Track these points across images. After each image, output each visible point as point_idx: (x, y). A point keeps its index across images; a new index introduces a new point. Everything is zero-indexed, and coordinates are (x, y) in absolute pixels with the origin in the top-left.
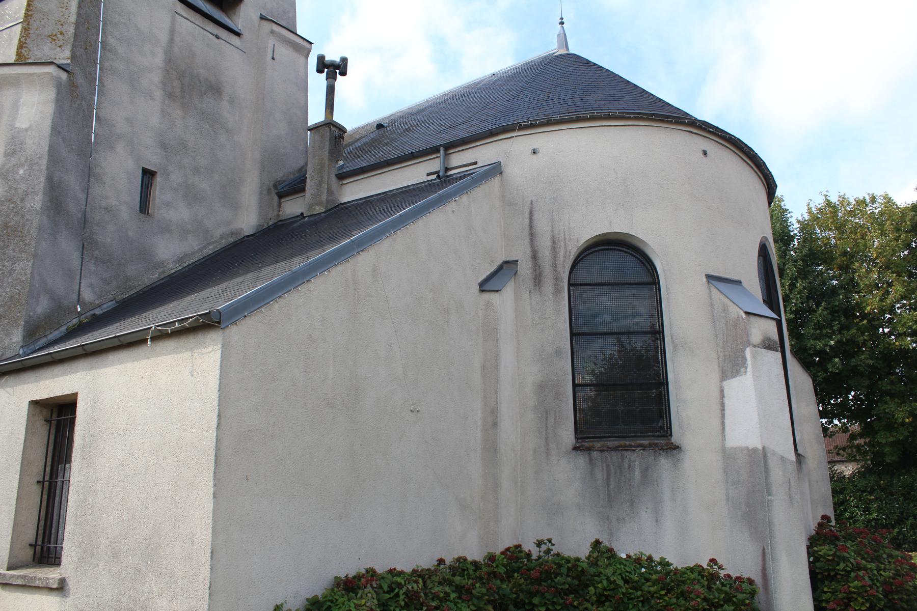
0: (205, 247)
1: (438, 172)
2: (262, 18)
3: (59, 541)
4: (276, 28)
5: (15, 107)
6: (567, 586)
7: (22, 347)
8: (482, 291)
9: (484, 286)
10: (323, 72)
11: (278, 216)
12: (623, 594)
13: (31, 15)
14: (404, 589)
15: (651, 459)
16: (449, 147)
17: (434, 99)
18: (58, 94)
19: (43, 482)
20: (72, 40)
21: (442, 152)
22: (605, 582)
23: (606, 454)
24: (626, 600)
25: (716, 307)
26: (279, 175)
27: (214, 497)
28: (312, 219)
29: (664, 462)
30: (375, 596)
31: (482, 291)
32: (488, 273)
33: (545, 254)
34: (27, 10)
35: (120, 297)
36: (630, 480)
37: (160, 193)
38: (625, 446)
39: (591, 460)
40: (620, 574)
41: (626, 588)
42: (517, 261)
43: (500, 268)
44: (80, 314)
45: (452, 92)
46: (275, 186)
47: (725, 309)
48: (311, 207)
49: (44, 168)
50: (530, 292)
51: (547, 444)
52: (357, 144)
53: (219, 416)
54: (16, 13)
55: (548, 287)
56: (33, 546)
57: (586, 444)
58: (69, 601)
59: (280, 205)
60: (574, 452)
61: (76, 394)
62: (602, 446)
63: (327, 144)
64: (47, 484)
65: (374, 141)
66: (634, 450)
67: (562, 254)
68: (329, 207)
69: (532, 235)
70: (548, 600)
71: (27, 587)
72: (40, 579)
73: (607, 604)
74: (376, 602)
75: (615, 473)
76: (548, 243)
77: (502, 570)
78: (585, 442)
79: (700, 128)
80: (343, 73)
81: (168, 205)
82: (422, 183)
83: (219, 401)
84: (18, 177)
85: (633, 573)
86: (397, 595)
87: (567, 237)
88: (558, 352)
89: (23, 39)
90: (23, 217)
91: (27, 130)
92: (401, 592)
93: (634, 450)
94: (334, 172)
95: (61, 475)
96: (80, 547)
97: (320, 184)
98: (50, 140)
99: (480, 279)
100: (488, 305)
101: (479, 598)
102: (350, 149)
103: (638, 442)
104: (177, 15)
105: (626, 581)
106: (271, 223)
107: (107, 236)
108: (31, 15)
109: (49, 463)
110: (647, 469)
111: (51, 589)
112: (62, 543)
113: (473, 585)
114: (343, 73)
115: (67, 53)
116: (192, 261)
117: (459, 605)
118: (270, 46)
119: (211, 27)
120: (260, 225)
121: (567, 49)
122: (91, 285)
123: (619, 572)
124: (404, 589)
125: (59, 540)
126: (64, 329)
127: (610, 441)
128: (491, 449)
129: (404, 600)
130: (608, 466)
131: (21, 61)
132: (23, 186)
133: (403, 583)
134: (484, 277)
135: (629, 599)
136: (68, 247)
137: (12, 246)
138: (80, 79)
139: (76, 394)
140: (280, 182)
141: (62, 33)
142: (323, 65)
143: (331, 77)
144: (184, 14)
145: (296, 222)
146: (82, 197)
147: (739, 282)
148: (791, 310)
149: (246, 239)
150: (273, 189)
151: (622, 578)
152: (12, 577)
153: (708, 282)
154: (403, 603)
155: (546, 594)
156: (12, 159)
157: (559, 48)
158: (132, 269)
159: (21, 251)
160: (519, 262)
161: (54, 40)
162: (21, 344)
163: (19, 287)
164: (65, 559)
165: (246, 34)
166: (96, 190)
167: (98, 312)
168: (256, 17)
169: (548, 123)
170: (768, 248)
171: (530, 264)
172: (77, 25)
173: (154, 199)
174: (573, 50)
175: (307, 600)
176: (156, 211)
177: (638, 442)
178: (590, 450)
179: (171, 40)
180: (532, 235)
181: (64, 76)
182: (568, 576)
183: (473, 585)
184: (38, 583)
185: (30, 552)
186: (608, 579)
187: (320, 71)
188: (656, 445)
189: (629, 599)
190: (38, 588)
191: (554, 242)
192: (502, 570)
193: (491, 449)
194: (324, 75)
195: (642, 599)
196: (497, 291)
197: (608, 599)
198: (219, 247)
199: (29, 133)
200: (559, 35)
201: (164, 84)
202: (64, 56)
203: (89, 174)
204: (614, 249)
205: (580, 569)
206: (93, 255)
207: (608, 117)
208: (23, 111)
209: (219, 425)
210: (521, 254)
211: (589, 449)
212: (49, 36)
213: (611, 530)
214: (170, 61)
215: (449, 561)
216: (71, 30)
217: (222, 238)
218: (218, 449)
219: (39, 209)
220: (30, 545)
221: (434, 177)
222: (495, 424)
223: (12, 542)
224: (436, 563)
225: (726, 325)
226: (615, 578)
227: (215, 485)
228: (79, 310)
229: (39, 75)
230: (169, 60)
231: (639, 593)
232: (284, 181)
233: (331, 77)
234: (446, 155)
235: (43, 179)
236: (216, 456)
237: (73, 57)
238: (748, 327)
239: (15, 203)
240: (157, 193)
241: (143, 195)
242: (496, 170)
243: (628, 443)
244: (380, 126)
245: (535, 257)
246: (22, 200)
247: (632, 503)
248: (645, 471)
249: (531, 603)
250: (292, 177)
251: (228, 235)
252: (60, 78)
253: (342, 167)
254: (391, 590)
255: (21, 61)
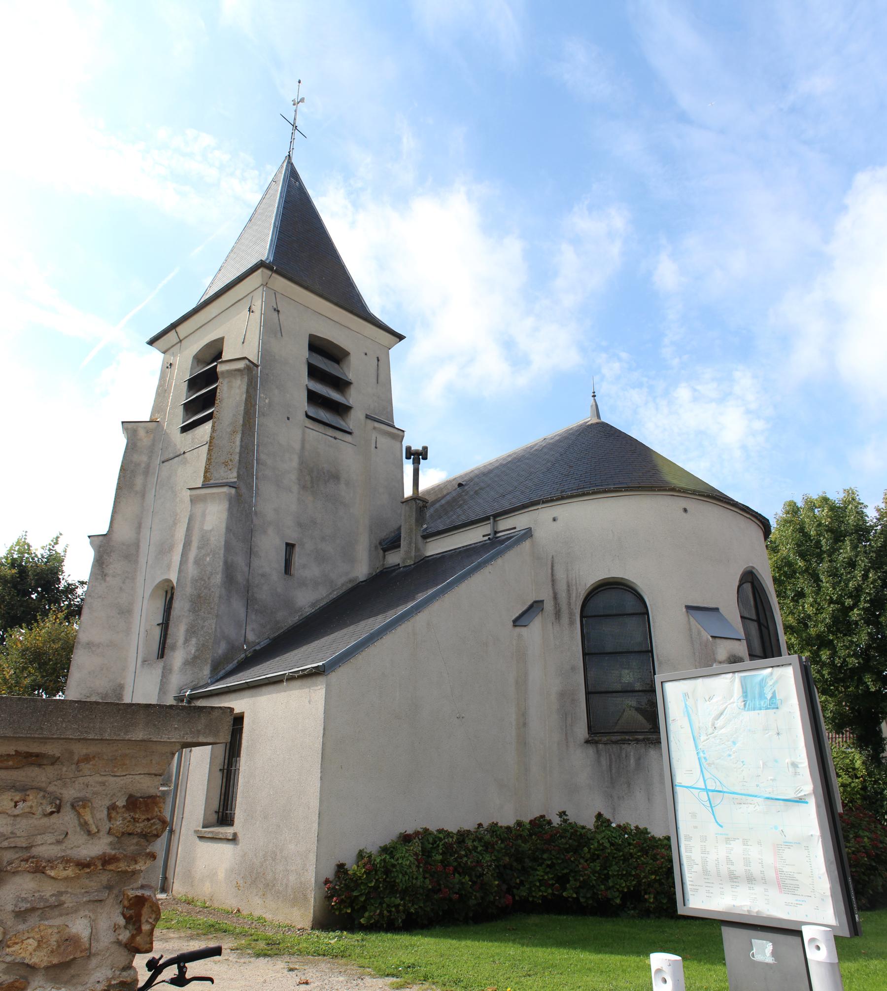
0: (330, 594)
1: (489, 535)
2: (368, 417)
3: (233, 810)
4: (377, 425)
5: (204, 515)
6: (568, 846)
7: (210, 678)
8: (515, 626)
9: (516, 622)
10: (410, 458)
11: (383, 565)
12: (609, 854)
13: (212, 449)
14: (443, 842)
15: (643, 750)
16: (496, 516)
17: (501, 459)
18: (230, 504)
19: (224, 769)
20: (238, 464)
21: (492, 520)
22: (596, 844)
23: (609, 746)
24: (611, 858)
25: (693, 631)
26: (383, 535)
27: (321, 779)
28: (405, 569)
29: (652, 753)
30: (420, 845)
31: (515, 626)
32: (520, 612)
33: (563, 595)
34: (205, 477)
35: (272, 636)
36: (626, 767)
37: (298, 559)
38: (624, 740)
39: (598, 751)
40: (607, 838)
41: (612, 849)
42: (543, 601)
43: (531, 606)
44: (246, 650)
45: (515, 453)
46: (380, 543)
47: (699, 633)
48: (404, 560)
49: (222, 555)
50: (553, 623)
51: (567, 739)
52: (443, 502)
53: (324, 729)
54: (201, 438)
55: (565, 619)
56: (217, 812)
57: (596, 738)
58: (239, 847)
59: (384, 557)
60: (585, 745)
61: (243, 713)
62: (608, 740)
63: (414, 513)
64: (225, 771)
65: (454, 500)
66: (629, 744)
67: (574, 595)
68: (417, 561)
69: (553, 581)
70: (554, 856)
71: (214, 839)
72: (222, 833)
73: (597, 861)
74: (420, 849)
75: (616, 761)
76: (565, 587)
77: (526, 833)
78: (596, 736)
79: (679, 491)
80: (425, 458)
81: (304, 566)
82: (480, 542)
83: (324, 720)
84: (206, 563)
85: (618, 838)
86: (438, 846)
87: (578, 582)
88: (573, 669)
89: (207, 466)
90: (210, 589)
91: (211, 531)
92: (441, 844)
93: (629, 744)
94: (420, 534)
95: (234, 764)
96: (245, 812)
97: (410, 543)
98: (225, 537)
99: (514, 618)
100: (520, 636)
101: (498, 851)
102: (437, 505)
103: (636, 737)
104: (306, 429)
105: (612, 844)
106: (378, 571)
107: (263, 594)
108: (212, 449)
109: (227, 757)
110: (639, 759)
111: (228, 840)
112: (234, 811)
113: (497, 842)
114: (425, 458)
115: (235, 474)
116: (322, 605)
117: (484, 856)
118: (374, 438)
119: (331, 432)
120: (370, 574)
121: (598, 416)
122: (253, 630)
123: (607, 837)
124: (443, 842)
125: (232, 808)
126: (236, 661)
127: (614, 736)
128: (523, 742)
129: (442, 849)
130: (610, 755)
131: (204, 486)
132: (209, 569)
133: (443, 837)
134: (517, 615)
135: (613, 858)
136: (238, 606)
137: (203, 610)
138: (243, 490)
139: (243, 713)
140: (384, 540)
141: (231, 460)
142: (410, 453)
143: (416, 462)
144: (311, 427)
145: (394, 570)
146: (246, 569)
147: (716, 610)
148: (865, 599)
149: (361, 584)
150: (379, 546)
151: (609, 841)
152: (205, 832)
153: (687, 612)
154: (441, 851)
155: (553, 851)
156: (203, 551)
157: (591, 417)
158: (280, 615)
159: (209, 613)
160: (545, 601)
161: (227, 465)
162: (209, 676)
163: (207, 638)
164: (237, 821)
165: (356, 432)
166: (256, 563)
167: (258, 648)
168: (362, 417)
169: (563, 498)
170: (756, 574)
171: (552, 603)
172: (240, 453)
173: (294, 563)
174: (604, 419)
175: (380, 847)
176: (296, 572)
177: (636, 737)
178: (597, 743)
179: (303, 447)
180: (553, 581)
181: (233, 491)
182: (570, 838)
183: (497, 842)
184: (221, 836)
185: (215, 817)
186: (598, 842)
187: (408, 458)
188: (648, 739)
189: (613, 858)
190: (220, 839)
191: (568, 586)
192: (526, 833)
193: (523, 742)
194: (411, 460)
195: (622, 858)
196: (525, 626)
197: (598, 857)
198: (341, 592)
199: (212, 533)
200: (592, 406)
201: (299, 480)
202: (232, 477)
203: (251, 552)
204: (617, 588)
205: (578, 833)
206: (254, 608)
207: (605, 492)
208: (208, 518)
209: (324, 734)
210: (545, 595)
211: (596, 743)
212: (223, 463)
213: (614, 806)
214: (302, 463)
215: (485, 825)
216: (237, 458)
217: (343, 585)
218: (323, 749)
219: (219, 584)
220: (216, 812)
221: (486, 538)
222: (525, 724)
223: (205, 810)
224: (477, 826)
225: (701, 645)
226: (603, 841)
227: (321, 772)
228: (245, 648)
229: (218, 493)
230: (302, 462)
231: (621, 853)
232: (387, 539)
233: (416, 462)
234: (495, 521)
235: (221, 564)
236: (322, 754)
237: (238, 477)
238: (714, 648)
239: (204, 580)
240: (296, 559)
241: (184, 788)
242: (528, 533)
243: (627, 737)
244: (460, 485)
245: (555, 597)
246: (209, 578)
247: (629, 785)
248: (638, 760)
249: (542, 858)
250: (393, 534)
251: (348, 582)
252: (231, 493)
253: (426, 529)
254: (435, 842)
255: (204, 486)
